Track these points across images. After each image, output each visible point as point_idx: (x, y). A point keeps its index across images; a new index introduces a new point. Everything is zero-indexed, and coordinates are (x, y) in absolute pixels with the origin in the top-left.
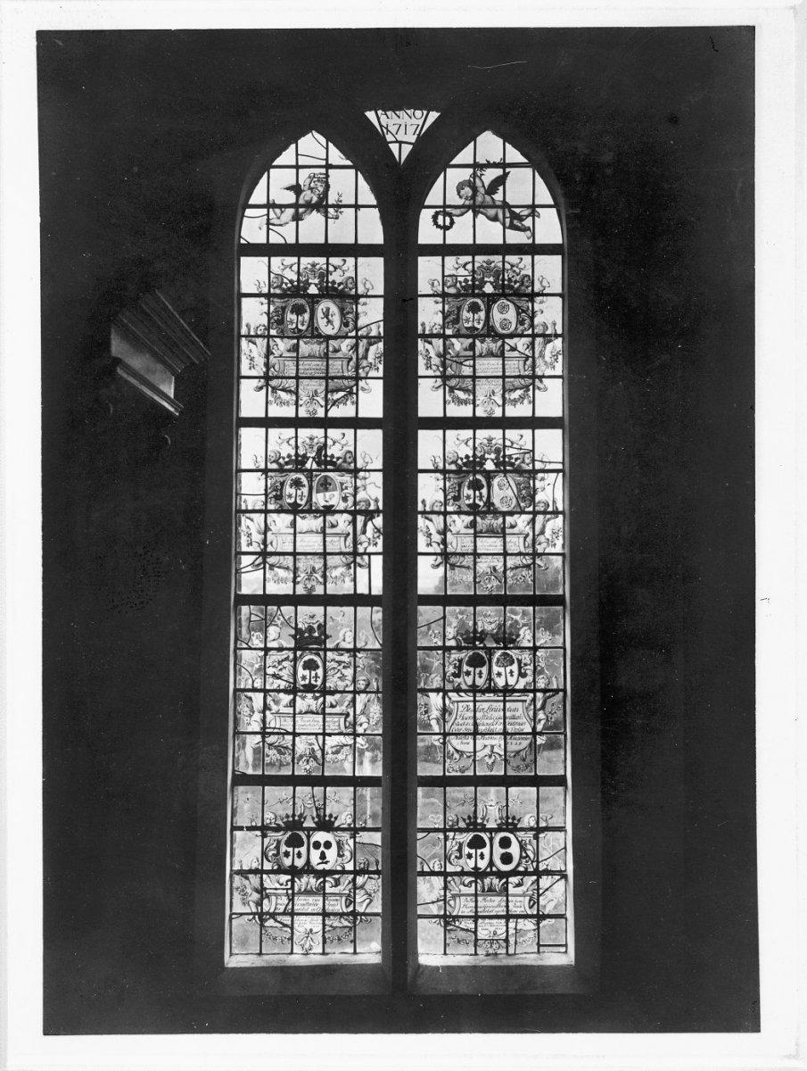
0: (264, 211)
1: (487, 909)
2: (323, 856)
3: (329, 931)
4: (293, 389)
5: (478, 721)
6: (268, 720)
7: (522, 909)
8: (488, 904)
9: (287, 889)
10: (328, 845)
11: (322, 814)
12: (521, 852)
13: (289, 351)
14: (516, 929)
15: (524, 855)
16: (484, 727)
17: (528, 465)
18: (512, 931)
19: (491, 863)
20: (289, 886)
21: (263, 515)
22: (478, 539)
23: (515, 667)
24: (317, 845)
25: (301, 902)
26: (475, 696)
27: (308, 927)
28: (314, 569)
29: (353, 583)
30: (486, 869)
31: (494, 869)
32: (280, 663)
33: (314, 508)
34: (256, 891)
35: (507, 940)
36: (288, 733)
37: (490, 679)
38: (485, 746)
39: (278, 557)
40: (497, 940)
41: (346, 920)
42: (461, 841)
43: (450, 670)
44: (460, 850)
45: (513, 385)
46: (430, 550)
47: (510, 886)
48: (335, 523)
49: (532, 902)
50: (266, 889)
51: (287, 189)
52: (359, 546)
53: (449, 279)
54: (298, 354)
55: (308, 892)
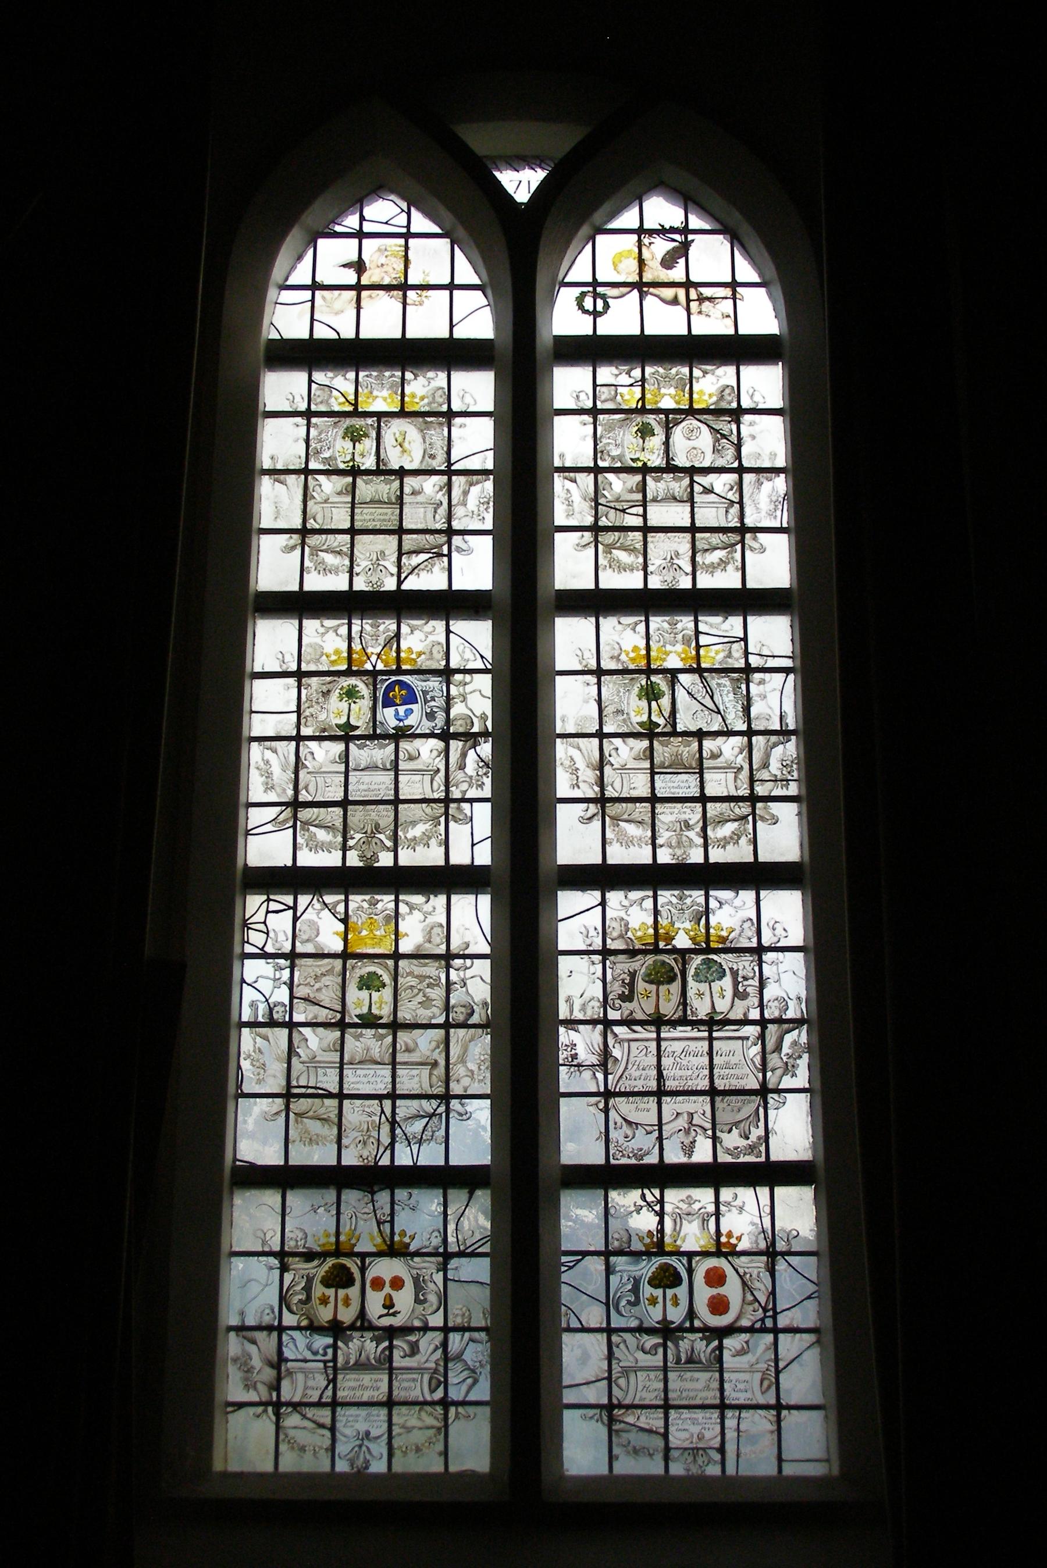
0: (307, 295)
1: (684, 1394)
2: (389, 1304)
3: (400, 1435)
4: (345, 549)
5: (665, 1073)
6: (294, 1074)
7: (749, 1395)
8: (688, 1385)
9: (325, 1362)
10: (397, 1283)
11: (388, 1231)
12: (744, 1294)
13: (339, 493)
14: (738, 1430)
15: (750, 1298)
16: (676, 1083)
17: (737, 660)
18: (731, 1435)
19: (691, 1314)
20: (329, 1356)
21: (294, 743)
22: (657, 777)
23: (727, 982)
24: (378, 1284)
25: (352, 1384)
26: (658, 1033)
27: (362, 1427)
28: (377, 827)
29: (443, 848)
30: (683, 1322)
31: (697, 1323)
32: (317, 978)
33: (378, 731)
34: (271, 1365)
35: (722, 1450)
36: (330, 1095)
37: (684, 1002)
38: (678, 1114)
39: (315, 810)
40: (704, 1449)
41: (431, 1414)
42: (639, 1273)
43: (616, 989)
44: (636, 1290)
45: (709, 543)
46: (577, 794)
47: (726, 1355)
48: (415, 753)
49: (766, 1383)
50: (287, 1360)
51: (344, 266)
52: (453, 789)
53: (604, 389)
54: (353, 498)
55: (361, 1366)
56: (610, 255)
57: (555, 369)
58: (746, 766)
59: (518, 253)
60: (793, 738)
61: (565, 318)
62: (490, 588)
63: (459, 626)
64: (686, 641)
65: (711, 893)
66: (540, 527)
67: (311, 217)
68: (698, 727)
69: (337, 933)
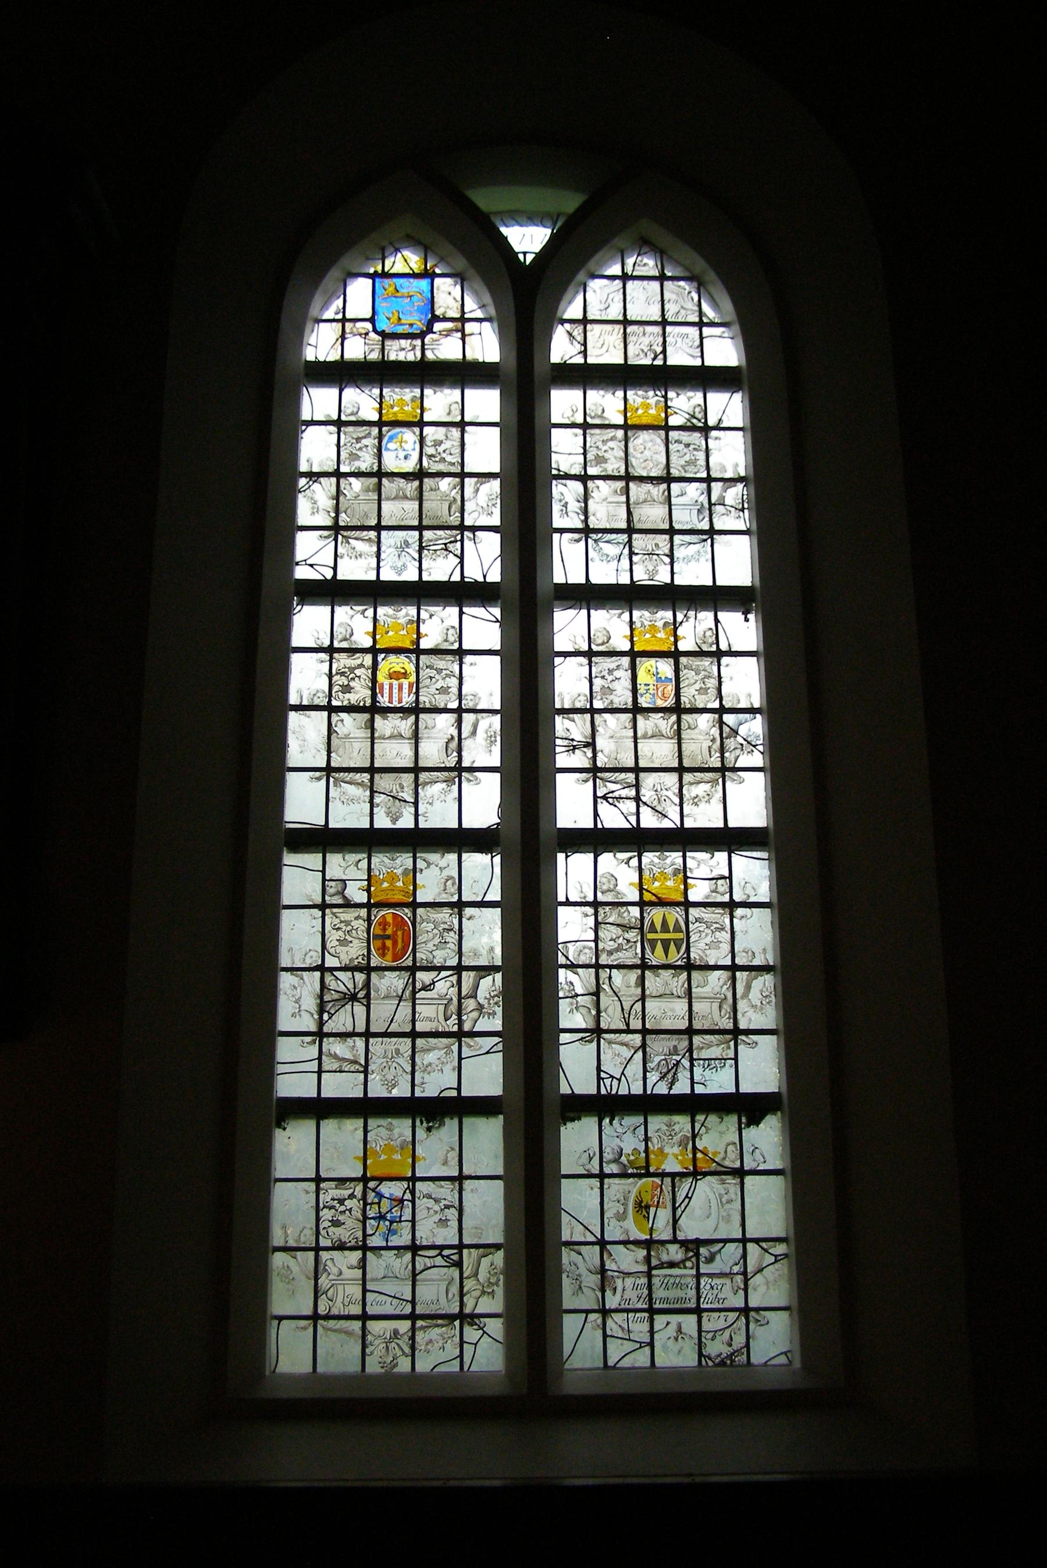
32: (358, 440)
56: (599, 296)
58: (730, 995)
60: (758, 716)
61: (562, 348)
64: (683, 1144)
65: (688, 854)
67: (347, 262)
68: (684, 738)
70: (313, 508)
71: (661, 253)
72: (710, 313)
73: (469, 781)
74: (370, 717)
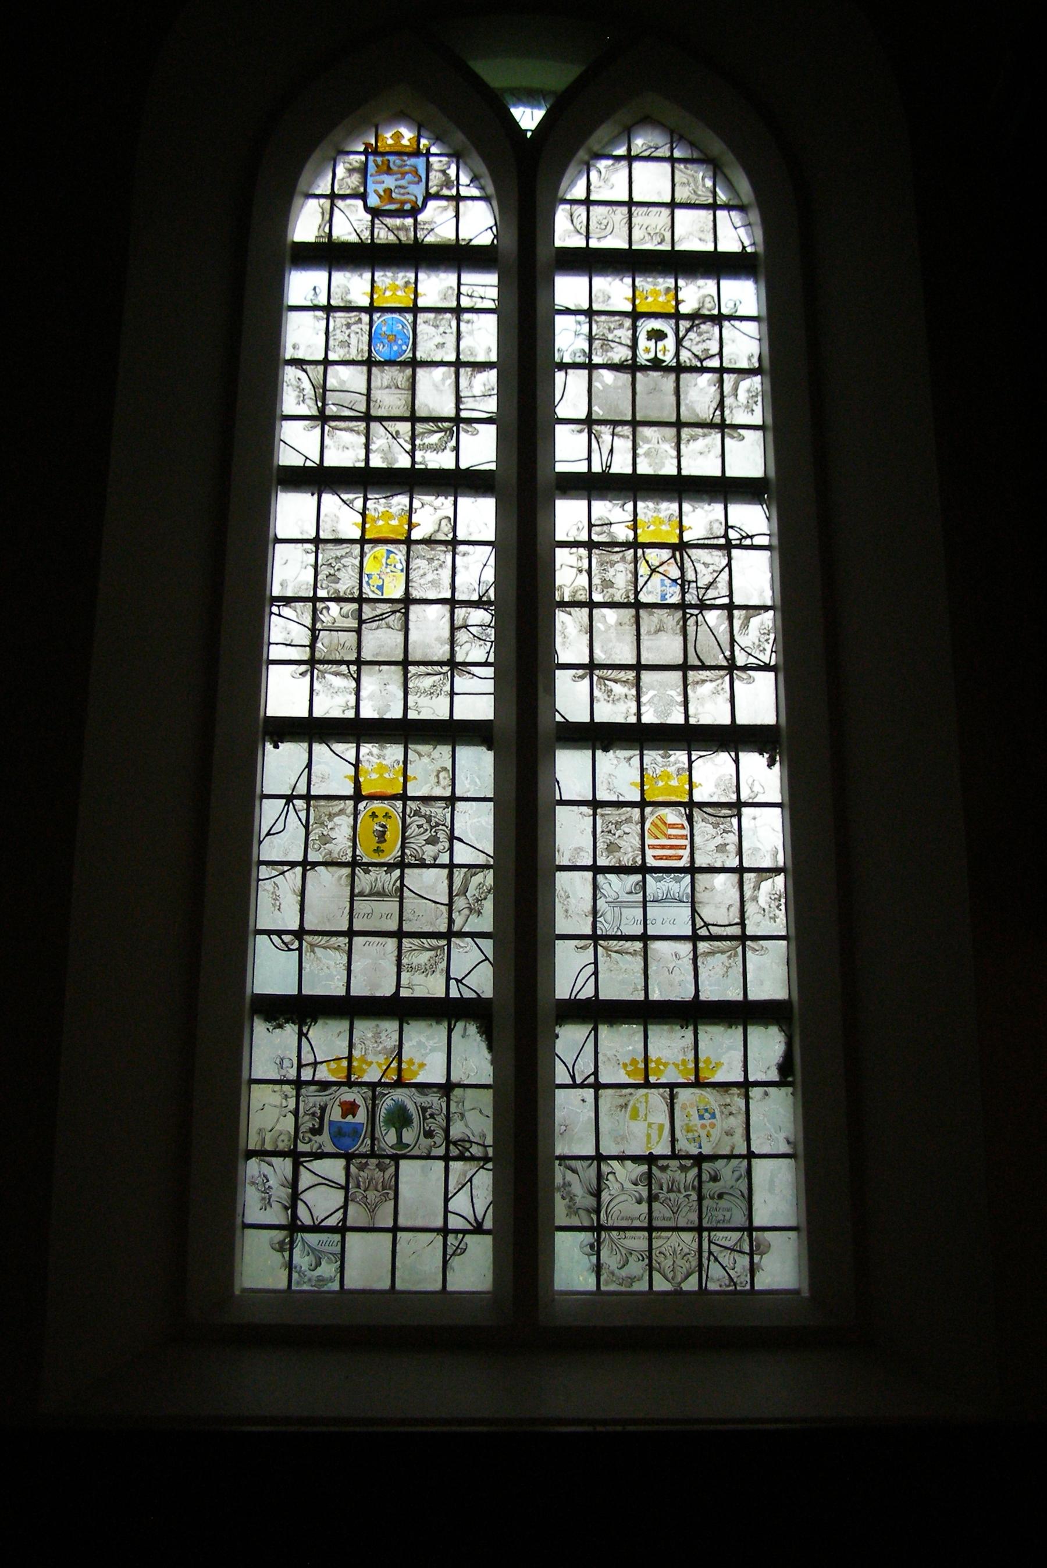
46: (575, 1222)
49: (737, 1174)
57: (557, 752)
59: (525, 179)
61: (566, 232)
62: (491, 717)
63: (466, 503)
66: (541, 932)
68: (692, 609)
69: (356, 524)
70: (299, 397)
71: (676, 136)
72: (722, 197)
73: (467, 432)
74: (356, 601)
